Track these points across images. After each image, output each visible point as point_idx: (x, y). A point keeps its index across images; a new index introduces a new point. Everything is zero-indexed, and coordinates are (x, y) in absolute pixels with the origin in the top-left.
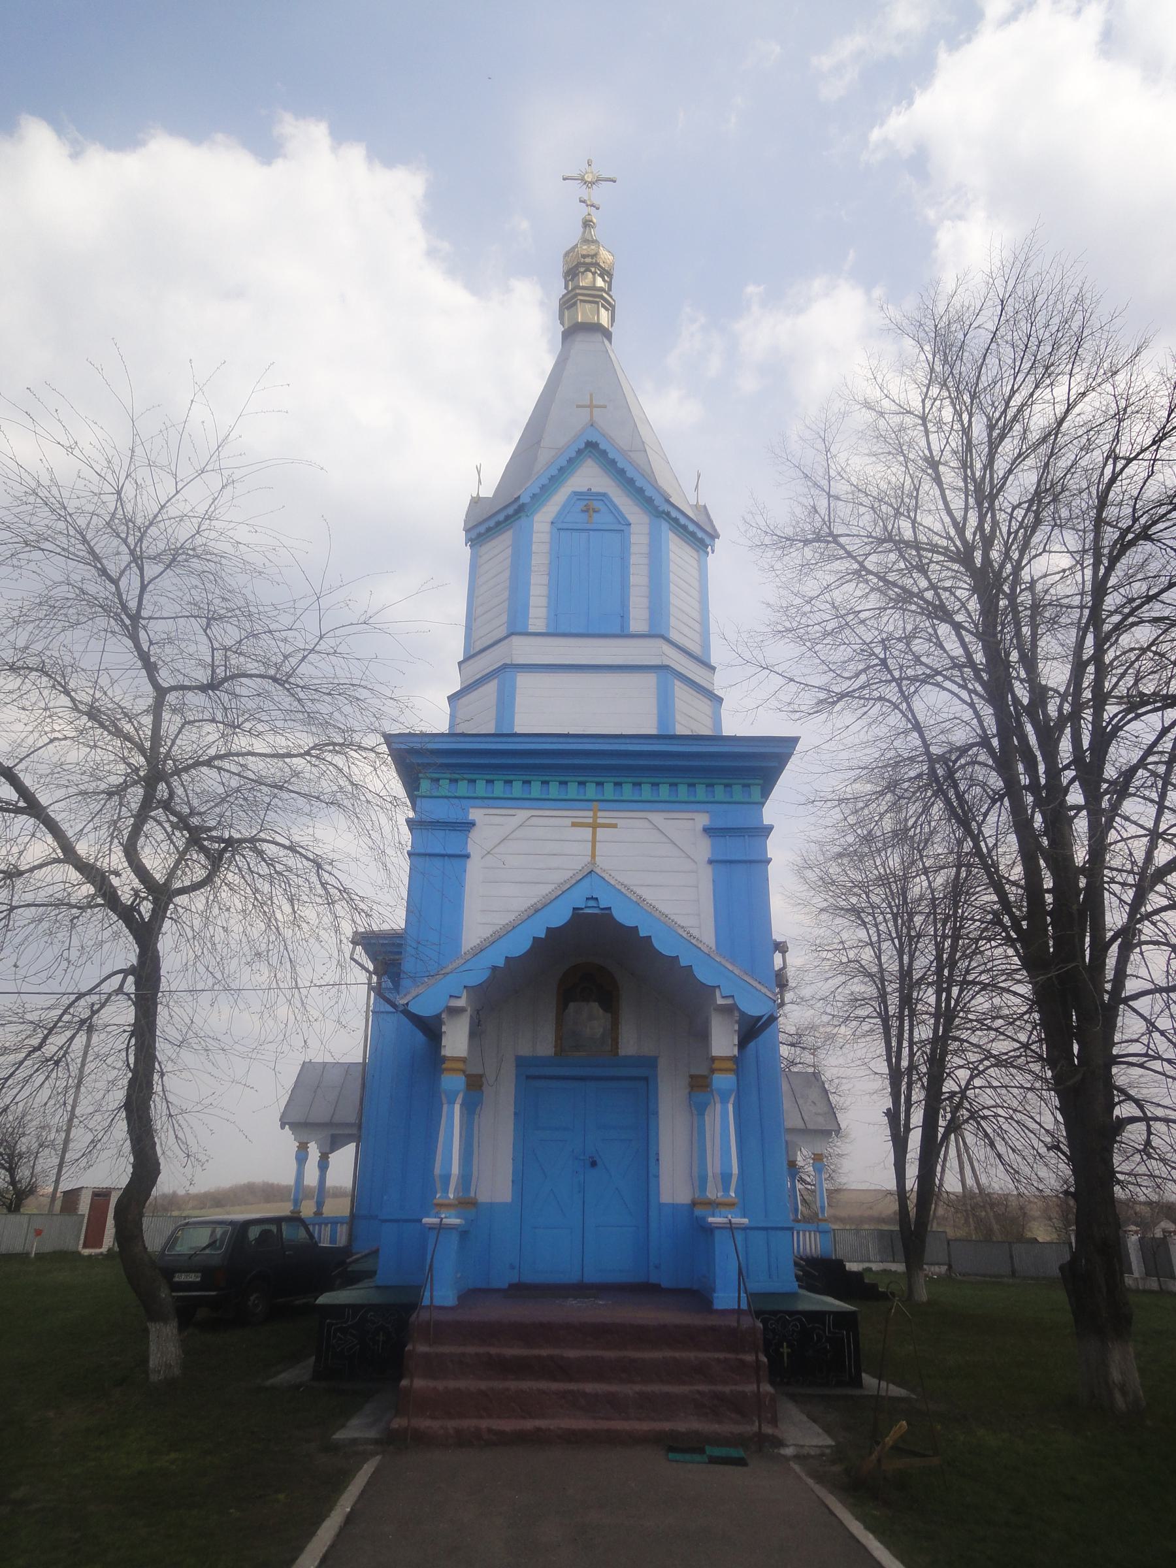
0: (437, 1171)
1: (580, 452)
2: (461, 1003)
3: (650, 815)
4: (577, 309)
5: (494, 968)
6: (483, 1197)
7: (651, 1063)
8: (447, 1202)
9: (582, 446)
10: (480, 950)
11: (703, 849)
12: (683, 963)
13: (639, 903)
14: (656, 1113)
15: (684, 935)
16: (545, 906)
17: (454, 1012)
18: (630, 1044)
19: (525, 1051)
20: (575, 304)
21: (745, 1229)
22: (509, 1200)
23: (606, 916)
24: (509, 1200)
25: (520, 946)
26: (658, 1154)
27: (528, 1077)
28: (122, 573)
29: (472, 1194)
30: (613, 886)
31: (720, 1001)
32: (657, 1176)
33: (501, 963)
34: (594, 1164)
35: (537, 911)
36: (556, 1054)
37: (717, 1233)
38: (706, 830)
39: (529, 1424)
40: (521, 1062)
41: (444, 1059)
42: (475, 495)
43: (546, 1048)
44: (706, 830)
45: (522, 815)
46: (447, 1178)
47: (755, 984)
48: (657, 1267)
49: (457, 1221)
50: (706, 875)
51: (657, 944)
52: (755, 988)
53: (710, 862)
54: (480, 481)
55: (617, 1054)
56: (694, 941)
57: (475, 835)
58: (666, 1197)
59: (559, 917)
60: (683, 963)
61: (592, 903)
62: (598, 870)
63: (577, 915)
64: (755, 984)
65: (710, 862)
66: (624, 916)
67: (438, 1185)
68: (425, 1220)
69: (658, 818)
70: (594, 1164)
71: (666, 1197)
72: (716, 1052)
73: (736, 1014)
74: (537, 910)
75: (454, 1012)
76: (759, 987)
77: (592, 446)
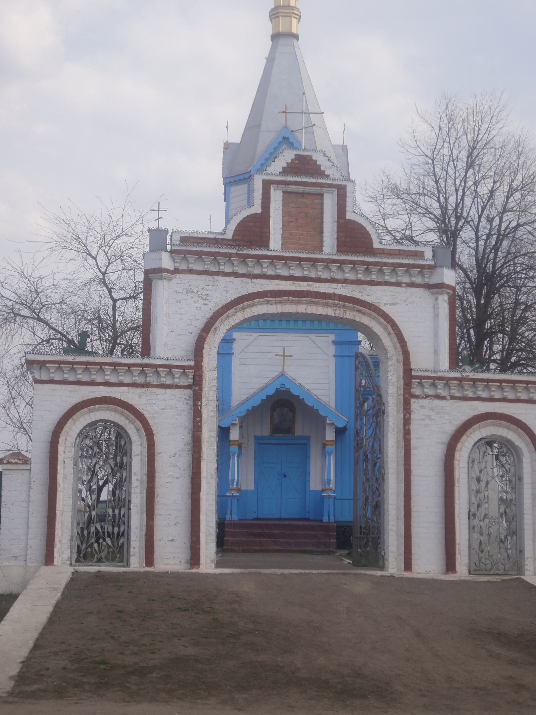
0: (230, 478)
1: (280, 143)
2: (237, 422)
3: (310, 335)
4: (279, 19)
5: (248, 410)
6: (243, 487)
7: (308, 438)
8: (233, 488)
9: (281, 140)
10: (243, 403)
11: (332, 350)
12: (315, 408)
13: (300, 386)
14: (309, 458)
15: (316, 398)
16: (266, 387)
17: (233, 425)
18: (299, 431)
19: (258, 434)
20: (278, 17)
21: (335, 498)
22: (253, 489)
23: (288, 392)
24: (253, 489)
25: (257, 402)
26: (310, 472)
27: (259, 444)
28: (97, 255)
29: (239, 487)
30: (291, 380)
31: (328, 422)
32: (309, 481)
33: (250, 408)
34: (285, 476)
35: (263, 389)
36: (270, 435)
37: (325, 498)
38: (334, 342)
39: (263, 548)
40: (256, 438)
41: (230, 441)
42: (225, 142)
43: (266, 432)
44: (334, 342)
45: (255, 335)
46: (233, 481)
47: (341, 416)
48: (309, 512)
49: (238, 494)
50: (333, 361)
51: (306, 402)
52: (341, 417)
53: (335, 356)
54: (227, 127)
55: (294, 435)
56: (319, 400)
57: (235, 345)
58: (312, 488)
59: (271, 391)
60: (315, 408)
61: (283, 386)
62: (285, 374)
63: (277, 391)
64: (341, 416)
65: (335, 356)
66: (295, 392)
67: (230, 483)
68: (227, 494)
69: (313, 336)
70: (285, 476)
71: (312, 488)
72: (327, 439)
73: (334, 426)
74: (262, 389)
75: (233, 425)
76: (342, 417)
77: (285, 139)
